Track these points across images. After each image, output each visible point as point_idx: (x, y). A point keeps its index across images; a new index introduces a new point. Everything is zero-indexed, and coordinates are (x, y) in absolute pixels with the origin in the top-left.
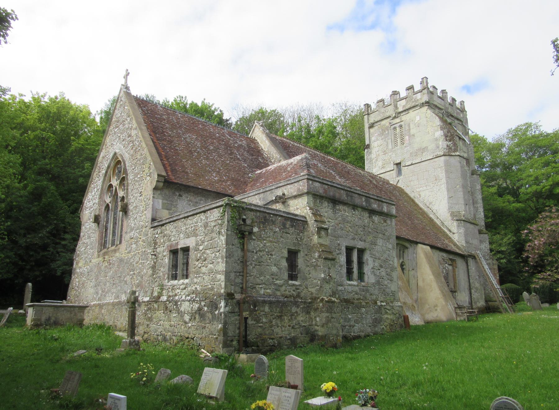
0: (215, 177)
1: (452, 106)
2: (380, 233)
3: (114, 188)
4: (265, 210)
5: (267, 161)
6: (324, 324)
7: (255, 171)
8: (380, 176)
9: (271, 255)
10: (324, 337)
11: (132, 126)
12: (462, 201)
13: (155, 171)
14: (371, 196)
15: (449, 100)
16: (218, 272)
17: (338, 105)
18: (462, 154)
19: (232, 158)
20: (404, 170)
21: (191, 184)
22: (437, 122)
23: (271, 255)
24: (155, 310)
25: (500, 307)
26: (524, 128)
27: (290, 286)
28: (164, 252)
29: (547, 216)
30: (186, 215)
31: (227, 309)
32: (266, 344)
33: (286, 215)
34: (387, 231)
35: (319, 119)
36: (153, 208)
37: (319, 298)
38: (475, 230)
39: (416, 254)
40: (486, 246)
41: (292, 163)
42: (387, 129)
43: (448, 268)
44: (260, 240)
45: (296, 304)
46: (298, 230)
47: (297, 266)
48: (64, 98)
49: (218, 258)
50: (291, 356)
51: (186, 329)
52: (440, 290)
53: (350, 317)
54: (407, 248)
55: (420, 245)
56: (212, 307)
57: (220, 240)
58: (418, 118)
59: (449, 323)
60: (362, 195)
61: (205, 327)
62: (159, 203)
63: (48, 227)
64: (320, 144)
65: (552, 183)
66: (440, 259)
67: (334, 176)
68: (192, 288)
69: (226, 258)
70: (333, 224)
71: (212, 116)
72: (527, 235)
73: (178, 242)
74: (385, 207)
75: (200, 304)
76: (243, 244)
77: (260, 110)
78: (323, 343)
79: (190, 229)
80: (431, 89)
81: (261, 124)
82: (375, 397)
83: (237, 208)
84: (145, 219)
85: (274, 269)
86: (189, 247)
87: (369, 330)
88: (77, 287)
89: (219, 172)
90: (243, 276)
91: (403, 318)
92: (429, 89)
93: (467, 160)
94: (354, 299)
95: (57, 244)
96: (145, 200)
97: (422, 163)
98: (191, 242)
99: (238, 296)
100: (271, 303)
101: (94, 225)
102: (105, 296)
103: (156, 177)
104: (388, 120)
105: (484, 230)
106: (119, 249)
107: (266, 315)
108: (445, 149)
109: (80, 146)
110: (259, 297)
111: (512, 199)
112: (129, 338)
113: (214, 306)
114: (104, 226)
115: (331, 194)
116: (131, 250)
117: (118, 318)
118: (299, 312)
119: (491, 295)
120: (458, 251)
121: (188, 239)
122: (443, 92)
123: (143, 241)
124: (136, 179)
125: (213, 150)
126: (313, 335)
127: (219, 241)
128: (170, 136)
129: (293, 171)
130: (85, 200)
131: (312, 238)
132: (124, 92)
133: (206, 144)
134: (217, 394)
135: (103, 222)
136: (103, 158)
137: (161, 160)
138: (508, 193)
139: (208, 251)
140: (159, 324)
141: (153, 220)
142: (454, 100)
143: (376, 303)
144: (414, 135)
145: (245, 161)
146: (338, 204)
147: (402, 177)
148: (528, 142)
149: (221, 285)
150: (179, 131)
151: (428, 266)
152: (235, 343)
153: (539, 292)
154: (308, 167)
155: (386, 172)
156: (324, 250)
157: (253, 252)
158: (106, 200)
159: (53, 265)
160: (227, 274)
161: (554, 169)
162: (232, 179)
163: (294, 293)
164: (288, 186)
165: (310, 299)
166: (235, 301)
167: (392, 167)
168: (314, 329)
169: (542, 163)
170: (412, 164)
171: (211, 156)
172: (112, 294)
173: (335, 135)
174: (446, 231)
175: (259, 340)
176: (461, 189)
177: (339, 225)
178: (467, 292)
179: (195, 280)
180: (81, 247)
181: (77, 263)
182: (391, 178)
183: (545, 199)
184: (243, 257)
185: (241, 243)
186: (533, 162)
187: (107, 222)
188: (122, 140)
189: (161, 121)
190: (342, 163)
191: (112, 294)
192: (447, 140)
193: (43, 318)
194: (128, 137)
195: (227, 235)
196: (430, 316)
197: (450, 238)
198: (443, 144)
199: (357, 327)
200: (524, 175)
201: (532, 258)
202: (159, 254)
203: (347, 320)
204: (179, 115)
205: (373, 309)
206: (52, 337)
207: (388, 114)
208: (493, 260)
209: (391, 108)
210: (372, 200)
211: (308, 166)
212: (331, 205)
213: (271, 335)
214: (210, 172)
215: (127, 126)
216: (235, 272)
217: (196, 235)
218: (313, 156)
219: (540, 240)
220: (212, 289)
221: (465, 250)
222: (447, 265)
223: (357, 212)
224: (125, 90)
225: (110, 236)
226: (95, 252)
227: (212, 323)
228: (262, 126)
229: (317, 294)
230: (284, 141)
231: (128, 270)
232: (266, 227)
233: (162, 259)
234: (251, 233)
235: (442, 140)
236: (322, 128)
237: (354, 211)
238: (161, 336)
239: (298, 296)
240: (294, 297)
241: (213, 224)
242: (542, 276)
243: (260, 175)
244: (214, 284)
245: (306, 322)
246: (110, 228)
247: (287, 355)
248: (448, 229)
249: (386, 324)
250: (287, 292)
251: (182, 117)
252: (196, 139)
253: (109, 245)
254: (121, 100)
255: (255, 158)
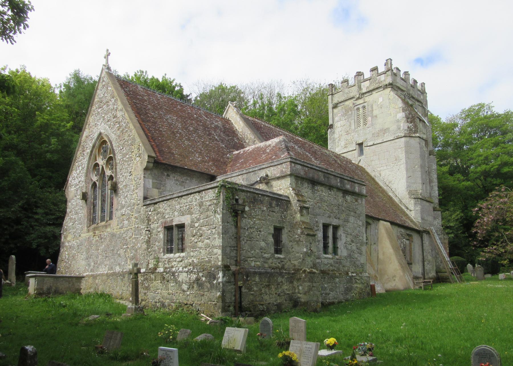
0: (198, 158)
1: (414, 88)
2: (352, 211)
3: (101, 167)
4: (254, 191)
5: (242, 141)
6: (306, 292)
7: (233, 152)
8: (342, 155)
9: (260, 231)
10: (306, 304)
11: (117, 108)
12: (419, 181)
13: (145, 152)
14: (345, 178)
15: (411, 82)
16: (214, 247)
17: (298, 83)
18: (421, 136)
19: (210, 139)
20: (366, 150)
21: (178, 165)
22: (400, 104)
23: (260, 231)
24: (151, 280)
25: (450, 278)
26: (477, 108)
27: (276, 259)
28: (158, 228)
29: (497, 195)
30: (180, 195)
31: (225, 279)
32: (257, 309)
33: (272, 195)
34: (358, 209)
35: (280, 97)
36: (144, 187)
37: (301, 269)
38: (430, 207)
39: (378, 230)
40: (438, 222)
41: (270, 145)
42: (350, 109)
43: (405, 242)
44: (251, 218)
45: (281, 274)
46: (282, 208)
47: (282, 241)
48: (24, 71)
49: (214, 234)
50: (295, 318)
51: (184, 296)
52: (399, 262)
53: (326, 286)
54: (370, 224)
55: (381, 222)
56: (210, 277)
57: (216, 218)
58: (381, 100)
59: (405, 292)
60: (337, 177)
61: (204, 294)
62: (150, 182)
63: (19, 202)
64: (282, 122)
65: (500, 162)
66: (399, 234)
67: (310, 158)
68: (189, 261)
69: (222, 234)
70: (312, 203)
71: (172, 92)
72: (477, 212)
73: (172, 219)
74: (357, 188)
75: (198, 275)
76: (237, 222)
77: (220, 86)
78: (305, 308)
79: (185, 208)
80: (395, 71)
81: (234, 105)
82: (373, 348)
83: (231, 189)
84: (136, 197)
85: (263, 244)
86: (184, 224)
87: (342, 297)
88: (67, 259)
89: (200, 153)
90: (237, 250)
91: (370, 287)
92: (393, 71)
93: (426, 141)
94: (329, 270)
95: (29, 217)
96: (136, 179)
97: (383, 143)
98: (186, 220)
99: (233, 268)
100: (260, 274)
101: (81, 203)
102: (98, 268)
103: (147, 158)
104: (352, 100)
105: (438, 207)
106: (110, 225)
107: (256, 284)
108: (405, 130)
109: (45, 121)
110: (251, 269)
111: (462, 178)
112: (134, 305)
113: (212, 276)
114: (91, 203)
115: (311, 175)
116: (123, 225)
117: (114, 287)
118: (284, 282)
119: (441, 267)
120: (414, 227)
121: (183, 217)
122: (406, 73)
123: (136, 218)
124: (125, 159)
125: (193, 130)
126: (296, 301)
127: (215, 219)
128: (153, 117)
129: (273, 153)
130: (69, 178)
131: (294, 216)
132: (106, 72)
133: (186, 125)
134: (240, 348)
135: (90, 199)
136: (87, 137)
137: (149, 141)
138: (459, 172)
139: (204, 228)
140: (157, 293)
141: (145, 198)
142: (415, 82)
143: (348, 274)
144: (376, 116)
145: (222, 142)
146: (316, 185)
147: (363, 157)
148: (480, 122)
149: (218, 258)
150: (161, 112)
151: (388, 241)
152: (231, 308)
153: (483, 264)
154: (287, 150)
155: (348, 152)
156: (307, 227)
157: (245, 229)
158: (92, 178)
159: (28, 238)
160: (224, 249)
161: (503, 149)
162: (213, 160)
163: (279, 265)
164: (272, 168)
165: (293, 270)
166: (231, 272)
167: (354, 146)
168: (297, 297)
169: (492, 143)
170: (374, 145)
171: (192, 137)
172: (106, 266)
173: (297, 113)
174: (403, 208)
175: (251, 305)
176: (419, 169)
177: (318, 204)
178: (421, 264)
179: (192, 254)
180: (68, 223)
181: (65, 238)
182: (353, 157)
183: (492, 178)
184: (237, 233)
185: (234, 221)
186: (484, 143)
187: (95, 199)
188: (107, 120)
189: (143, 103)
190: (309, 143)
191: (106, 266)
192: (408, 122)
193: (45, 288)
194: (114, 118)
195: (223, 214)
196: (390, 285)
197: (407, 215)
198: (404, 125)
199: (332, 295)
200: (475, 155)
201: (480, 235)
202: (153, 229)
203: (324, 289)
204: (159, 96)
205: (345, 279)
206: (60, 304)
207: (352, 95)
208: (444, 235)
209: (355, 88)
210: (346, 181)
211: (287, 149)
212: (310, 186)
213: (261, 301)
214: (193, 153)
215: (111, 107)
216: (230, 247)
217: (191, 213)
218: (291, 140)
219: (489, 217)
220: (209, 261)
221: (421, 226)
222: (404, 240)
223: (332, 192)
224: (107, 71)
225: (99, 213)
226: (84, 228)
227: (210, 291)
228: (235, 107)
229: (300, 266)
230: (256, 121)
231: (121, 244)
232: (255, 206)
233: (157, 235)
234: (243, 211)
235: (403, 121)
236: (284, 106)
237: (330, 191)
238: (160, 303)
239: (283, 267)
240: (279, 269)
241: (208, 203)
242: (489, 250)
243: (238, 156)
244: (211, 257)
245: (289, 290)
246: (98, 205)
247: (292, 316)
248: (406, 206)
249: (355, 292)
250: (274, 264)
251: (161, 98)
252: (177, 120)
253: (98, 220)
254: (103, 81)
255: (231, 139)
